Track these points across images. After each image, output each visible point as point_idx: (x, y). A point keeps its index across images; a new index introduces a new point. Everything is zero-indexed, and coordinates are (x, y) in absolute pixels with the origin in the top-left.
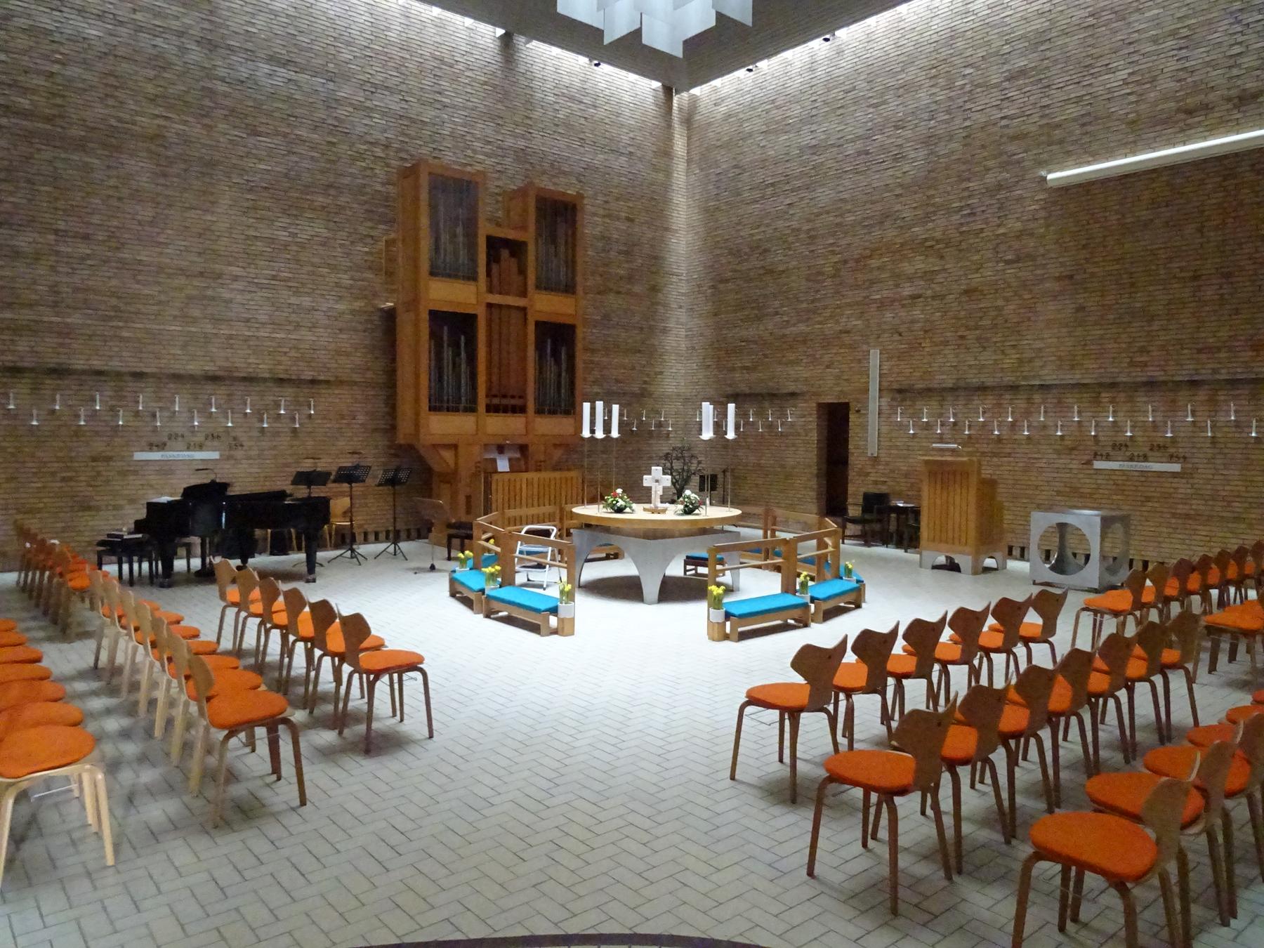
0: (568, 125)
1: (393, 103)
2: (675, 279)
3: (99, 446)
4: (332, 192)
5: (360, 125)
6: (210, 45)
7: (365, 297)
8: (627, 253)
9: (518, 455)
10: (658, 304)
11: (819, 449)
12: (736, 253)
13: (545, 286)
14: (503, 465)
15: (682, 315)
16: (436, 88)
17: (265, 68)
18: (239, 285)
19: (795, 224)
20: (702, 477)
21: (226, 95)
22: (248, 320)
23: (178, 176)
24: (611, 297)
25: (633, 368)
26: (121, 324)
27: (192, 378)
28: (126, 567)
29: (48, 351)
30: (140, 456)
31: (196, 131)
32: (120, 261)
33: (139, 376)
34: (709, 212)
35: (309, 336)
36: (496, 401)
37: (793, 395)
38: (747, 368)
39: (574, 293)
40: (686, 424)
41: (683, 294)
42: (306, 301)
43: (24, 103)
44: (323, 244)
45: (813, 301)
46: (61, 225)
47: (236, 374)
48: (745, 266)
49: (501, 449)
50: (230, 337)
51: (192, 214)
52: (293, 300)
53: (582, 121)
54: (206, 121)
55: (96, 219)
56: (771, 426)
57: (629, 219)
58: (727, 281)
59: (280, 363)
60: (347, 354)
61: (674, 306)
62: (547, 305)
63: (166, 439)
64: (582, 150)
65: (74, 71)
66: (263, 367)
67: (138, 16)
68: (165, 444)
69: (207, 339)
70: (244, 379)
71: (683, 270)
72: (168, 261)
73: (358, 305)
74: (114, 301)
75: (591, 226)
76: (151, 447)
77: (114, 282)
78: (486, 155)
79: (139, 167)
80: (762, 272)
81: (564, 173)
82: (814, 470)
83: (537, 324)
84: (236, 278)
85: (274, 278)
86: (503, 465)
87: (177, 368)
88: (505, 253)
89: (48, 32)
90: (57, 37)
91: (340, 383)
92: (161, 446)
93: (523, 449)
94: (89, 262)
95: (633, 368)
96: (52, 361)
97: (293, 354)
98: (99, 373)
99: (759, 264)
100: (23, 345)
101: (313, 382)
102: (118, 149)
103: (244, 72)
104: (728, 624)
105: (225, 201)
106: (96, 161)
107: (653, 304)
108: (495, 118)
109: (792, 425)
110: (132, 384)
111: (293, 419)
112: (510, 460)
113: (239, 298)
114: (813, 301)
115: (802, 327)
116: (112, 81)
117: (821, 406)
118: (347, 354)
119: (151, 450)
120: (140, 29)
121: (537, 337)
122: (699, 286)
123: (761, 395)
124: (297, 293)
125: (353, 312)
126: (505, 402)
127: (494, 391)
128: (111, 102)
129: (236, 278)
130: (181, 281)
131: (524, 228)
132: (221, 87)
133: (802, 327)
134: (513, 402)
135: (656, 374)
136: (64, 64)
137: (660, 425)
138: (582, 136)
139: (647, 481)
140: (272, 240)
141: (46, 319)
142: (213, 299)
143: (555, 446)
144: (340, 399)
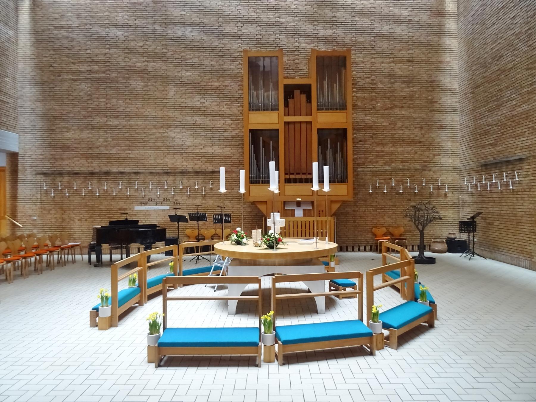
0: (363, 15)
1: (253, 29)
3: (121, 204)
4: (221, 79)
5: (235, 44)
6: (165, 25)
8: (409, 82)
12: (484, 66)
14: (299, 213)
15: (457, 116)
16: (277, 15)
17: (189, 29)
18: (178, 130)
19: (517, 30)
21: (173, 45)
22: (182, 145)
23: (153, 85)
24: (397, 111)
25: (416, 153)
26: (130, 152)
27: (158, 173)
28: (60, 256)
29: (96, 165)
30: (137, 208)
31: (160, 63)
32: (130, 125)
33: (137, 173)
34: (469, 44)
35: (210, 150)
36: (292, 177)
37: (521, 160)
38: (491, 144)
41: (456, 102)
42: (209, 134)
43: (96, 68)
44: (218, 105)
46: (109, 114)
47: (177, 171)
48: (490, 71)
49: (299, 204)
50: (174, 154)
51: (158, 101)
52: (203, 134)
53: (372, 10)
54: (165, 59)
55: (121, 109)
58: (479, 86)
60: (230, 158)
61: (449, 110)
62: (326, 119)
63: (147, 201)
64: (372, 26)
65: (112, 51)
66: (189, 166)
67: (137, 21)
68: (147, 203)
69: (165, 155)
70: (182, 172)
71: (456, 86)
72: (148, 123)
74: (128, 143)
75: (358, 68)
76: (142, 204)
77: (127, 135)
78: (306, 43)
79: (137, 85)
80: (499, 72)
81: (360, 43)
83: (319, 130)
84: (177, 126)
86: (299, 213)
87: (152, 169)
88: (297, 92)
89: (104, 38)
90: (107, 38)
92: (146, 204)
93: (312, 203)
94: (119, 127)
95: (416, 153)
96: (105, 169)
97: (203, 159)
98: (122, 173)
99: (496, 68)
100: (95, 164)
102: (129, 78)
103: (180, 33)
104: (277, 345)
105: (172, 92)
106: (121, 85)
108: (314, 22)
110: (134, 177)
113: (179, 136)
115: (525, 107)
116: (127, 51)
118: (230, 158)
119: (141, 206)
120: (137, 26)
122: (466, 94)
123: (501, 163)
124: (205, 130)
125: (233, 137)
126: (298, 177)
127: (291, 171)
128: (127, 60)
129: (177, 126)
130: (154, 131)
131: (309, 77)
132: (171, 42)
133: (525, 107)
135: (434, 155)
136: (109, 49)
138: (372, 18)
140: (192, 107)
141: (103, 152)
142: (167, 137)
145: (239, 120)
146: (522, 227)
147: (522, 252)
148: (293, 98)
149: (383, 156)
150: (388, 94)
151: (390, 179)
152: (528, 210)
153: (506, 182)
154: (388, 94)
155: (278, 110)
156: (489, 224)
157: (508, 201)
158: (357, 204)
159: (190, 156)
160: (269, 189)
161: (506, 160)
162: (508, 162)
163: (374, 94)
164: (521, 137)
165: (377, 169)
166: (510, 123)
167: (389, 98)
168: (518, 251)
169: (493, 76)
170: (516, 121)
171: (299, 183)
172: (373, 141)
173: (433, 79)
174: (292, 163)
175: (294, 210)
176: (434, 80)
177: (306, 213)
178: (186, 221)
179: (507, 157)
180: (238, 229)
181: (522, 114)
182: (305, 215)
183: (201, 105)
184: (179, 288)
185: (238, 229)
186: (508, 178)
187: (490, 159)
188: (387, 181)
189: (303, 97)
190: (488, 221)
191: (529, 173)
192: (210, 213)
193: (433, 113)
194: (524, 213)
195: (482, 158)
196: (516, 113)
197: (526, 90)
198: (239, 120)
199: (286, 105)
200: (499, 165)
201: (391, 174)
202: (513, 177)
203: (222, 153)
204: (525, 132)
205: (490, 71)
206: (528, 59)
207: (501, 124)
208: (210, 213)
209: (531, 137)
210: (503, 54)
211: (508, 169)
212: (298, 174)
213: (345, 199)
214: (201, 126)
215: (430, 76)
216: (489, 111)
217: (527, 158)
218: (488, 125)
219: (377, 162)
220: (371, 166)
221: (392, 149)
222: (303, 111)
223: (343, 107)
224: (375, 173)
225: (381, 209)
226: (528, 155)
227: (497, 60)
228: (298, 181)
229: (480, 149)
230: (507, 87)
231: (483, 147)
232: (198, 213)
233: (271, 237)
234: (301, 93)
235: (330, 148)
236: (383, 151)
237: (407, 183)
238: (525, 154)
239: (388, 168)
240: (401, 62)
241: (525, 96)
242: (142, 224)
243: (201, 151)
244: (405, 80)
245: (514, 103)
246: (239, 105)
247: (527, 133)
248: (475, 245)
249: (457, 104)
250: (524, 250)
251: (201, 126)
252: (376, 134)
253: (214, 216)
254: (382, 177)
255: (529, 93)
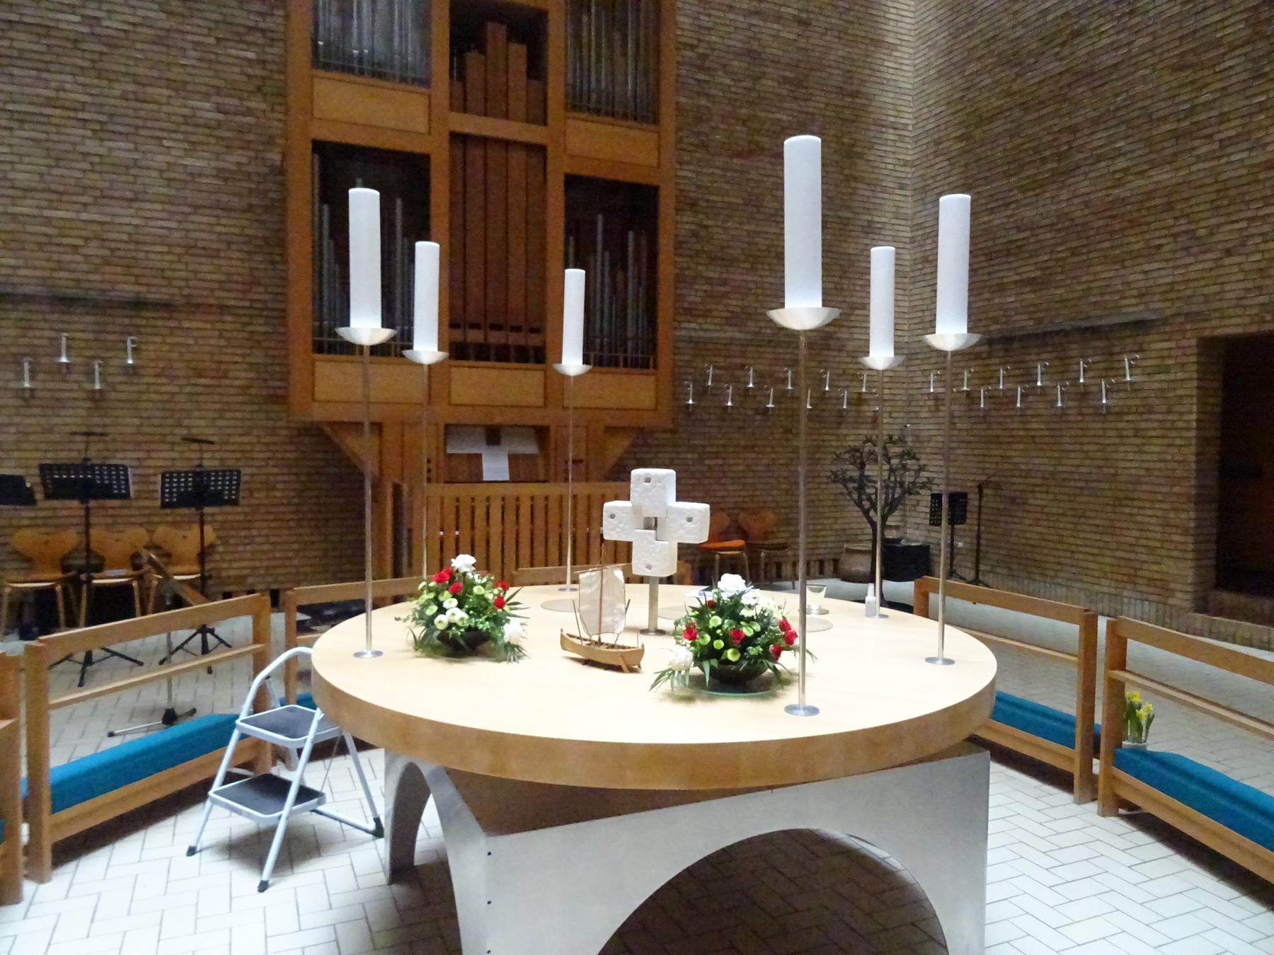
2: (891, 135)
7: (247, 145)
8: (799, 83)
9: (531, 449)
10: (855, 179)
11: (1203, 441)
12: (1014, 60)
13: (604, 107)
14: (495, 467)
20: (936, 498)
35: (127, 217)
36: (475, 336)
37: (1140, 326)
38: (1030, 281)
39: (656, 121)
40: (910, 400)
42: (121, 149)
45: (1191, 112)
48: (1033, 77)
49: (493, 436)
52: (92, 146)
56: (1084, 395)
57: (801, 22)
59: (60, 266)
62: (593, 145)
71: (907, 119)
73: (234, 159)
80: (1066, 79)
82: (1188, 487)
83: (572, 182)
85: (49, 102)
86: (495, 467)
88: (495, 32)
91: (194, 307)
93: (541, 434)
97: (93, 249)
99: (1055, 67)
101: (138, 305)
107: (848, 179)
109: (1135, 388)
111: (90, 374)
112: (513, 459)
114: (1191, 112)
115: (1163, 176)
117: (1207, 345)
121: (569, 208)
122: (937, 143)
124: (101, 132)
125: (221, 174)
126: (495, 338)
127: (472, 317)
133: (1163, 176)
134: (514, 339)
137: (859, 401)
139: (617, 519)
140: (45, 31)
143: (611, 430)
144: (200, 338)
145: (249, 112)
146: (1135, 511)
147: (1132, 579)
148: (482, 50)
149: (725, 295)
150: (743, 111)
151: (742, 367)
152: (1159, 465)
153: (968, 393)
154: (743, 111)
155: (425, 82)
156: (1013, 500)
157: (1087, 440)
158: (649, 441)
159: (30, 229)
160: (776, 315)
161: (1085, 324)
162: (1095, 331)
163: (703, 102)
164: (1140, 260)
165: (708, 335)
166: (1101, 223)
167: (744, 123)
168: (1120, 577)
169: (1046, 89)
170: (1128, 217)
171: (518, 361)
172: (698, 247)
173: (855, 88)
174: (475, 291)
175: (479, 457)
176: (858, 92)
177: (521, 470)
178: (26, 498)
179: (1088, 318)
180: (463, 562)
181: (1149, 195)
182: (515, 479)
183: (86, 30)
184: (28, 887)
185: (463, 562)
186: (1090, 374)
187: (1024, 323)
188: (734, 373)
189: (518, 52)
190: (1007, 493)
191: (1170, 362)
192: (147, 464)
193: (853, 184)
194: (1143, 472)
195: (995, 321)
196: (1128, 194)
197: (1168, 127)
198: (249, 112)
199: (458, 72)
200: (1057, 340)
201: (743, 354)
202: (1029, 376)
203: (176, 234)
204: (1160, 246)
205: (1033, 77)
206: (1181, 38)
207: (1067, 224)
208: (147, 464)
209: (1182, 262)
210: (1085, 26)
211: (1090, 352)
212: (496, 327)
213: (646, 421)
214: (81, 115)
215: (849, 75)
216: (1023, 189)
217: (1165, 321)
218: (1019, 230)
219: (706, 314)
220: (693, 325)
221: (750, 278)
222: (517, 105)
223: (645, 112)
224: (700, 347)
225: (717, 455)
226: (1169, 312)
227: (1063, 44)
228: (472, 352)
229: (987, 296)
230: (1096, 121)
231: (1001, 288)
232: (85, 466)
233: (738, 619)
234: (509, 39)
235: (604, 249)
236: (724, 282)
237: (785, 380)
238: (1158, 307)
239: (738, 335)
240: (779, 18)
241: (1165, 144)
242: (489, 35)
243: (84, 216)
244: (787, 74)
245: (1124, 165)
246: (250, 55)
247: (1167, 248)
248: (958, 558)
249: (908, 169)
250: (1140, 573)
251: (81, 115)
252: (706, 227)
253: (167, 476)
254: (721, 361)
255: (1177, 136)
